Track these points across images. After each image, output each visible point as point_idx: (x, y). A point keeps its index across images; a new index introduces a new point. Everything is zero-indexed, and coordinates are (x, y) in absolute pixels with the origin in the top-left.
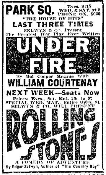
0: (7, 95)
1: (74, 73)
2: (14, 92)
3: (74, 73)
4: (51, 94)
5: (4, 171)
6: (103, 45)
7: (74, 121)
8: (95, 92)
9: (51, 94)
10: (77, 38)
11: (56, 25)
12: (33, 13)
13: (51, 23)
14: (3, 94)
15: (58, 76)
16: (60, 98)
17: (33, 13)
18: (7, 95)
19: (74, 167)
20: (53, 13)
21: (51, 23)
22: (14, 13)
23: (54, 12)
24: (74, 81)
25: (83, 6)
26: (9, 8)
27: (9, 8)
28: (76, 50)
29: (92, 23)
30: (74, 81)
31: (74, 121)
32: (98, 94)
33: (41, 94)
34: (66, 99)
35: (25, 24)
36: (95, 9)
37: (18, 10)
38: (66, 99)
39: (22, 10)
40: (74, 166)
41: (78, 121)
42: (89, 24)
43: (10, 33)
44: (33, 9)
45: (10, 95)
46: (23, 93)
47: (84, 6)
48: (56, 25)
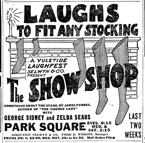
1: (132, 57)
2: (82, 125)
3: (132, 57)
4: (32, 129)
7: (116, 25)
8: (134, 119)
9: (32, 129)
10: (11, 43)
11: (46, 139)
12: (34, 130)
16: (96, 134)
17: (34, 130)
19: (97, 114)
23: (114, 138)
26: (8, 126)
28: (115, 65)
29: (41, 128)
31: (116, 25)
35: (43, 125)
36: (36, 105)
37: (83, 117)
39: (73, 127)
40: (52, 109)
41: (39, 99)
42: (88, 105)
48: (46, 139)
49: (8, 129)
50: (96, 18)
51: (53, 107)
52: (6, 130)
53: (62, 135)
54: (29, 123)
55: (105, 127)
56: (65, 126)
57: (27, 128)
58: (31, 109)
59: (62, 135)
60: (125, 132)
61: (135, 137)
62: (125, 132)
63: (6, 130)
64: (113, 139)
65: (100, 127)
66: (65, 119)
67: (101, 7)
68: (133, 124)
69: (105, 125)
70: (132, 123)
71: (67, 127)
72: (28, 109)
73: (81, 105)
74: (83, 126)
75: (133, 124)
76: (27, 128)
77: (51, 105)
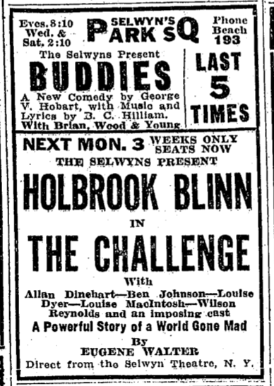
0: (25, 149)
4: (148, 38)
5: (251, 10)
6: (259, 184)
9: (148, 38)
13: (132, 32)
14: (186, 56)
15: (130, 304)
18: (25, 149)
20: (52, 35)
21: (132, 32)
22: (111, 41)
24: (39, 242)
25: (53, 23)
26: (97, 26)
27: (97, 26)
29: (165, 36)
30: (39, 242)
32: (142, 225)
33: (41, 146)
34: (36, 43)
38: (36, 43)
43: (223, 17)
44: (154, 33)
45: (32, 148)
46: (60, 144)
47: (57, 23)
49: (96, 35)
50: (4, 312)
51: (181, 357)
52: (45, 331)
53: (120, 57)
54: (210, 236)
55: (61, 34)
56: (113, 34)
57: (139, 37)
58: (217, 327)
59: (120, 57)
60: (155, 207)
61: (207, 206)
62: (155, 207)
63: (45, 331)
64: (49, 323)
65: (68, 44)
66: (161, 269)
67: (61, 330)
68: (42, 246)
69: (61, 28)
70: (40, 238)
71: (116, 35)
72: (104, 147)
73: (59, 329)
74: (137, 144)
75: (42, 246)
76: (139, 37)
77: (159, 349)
